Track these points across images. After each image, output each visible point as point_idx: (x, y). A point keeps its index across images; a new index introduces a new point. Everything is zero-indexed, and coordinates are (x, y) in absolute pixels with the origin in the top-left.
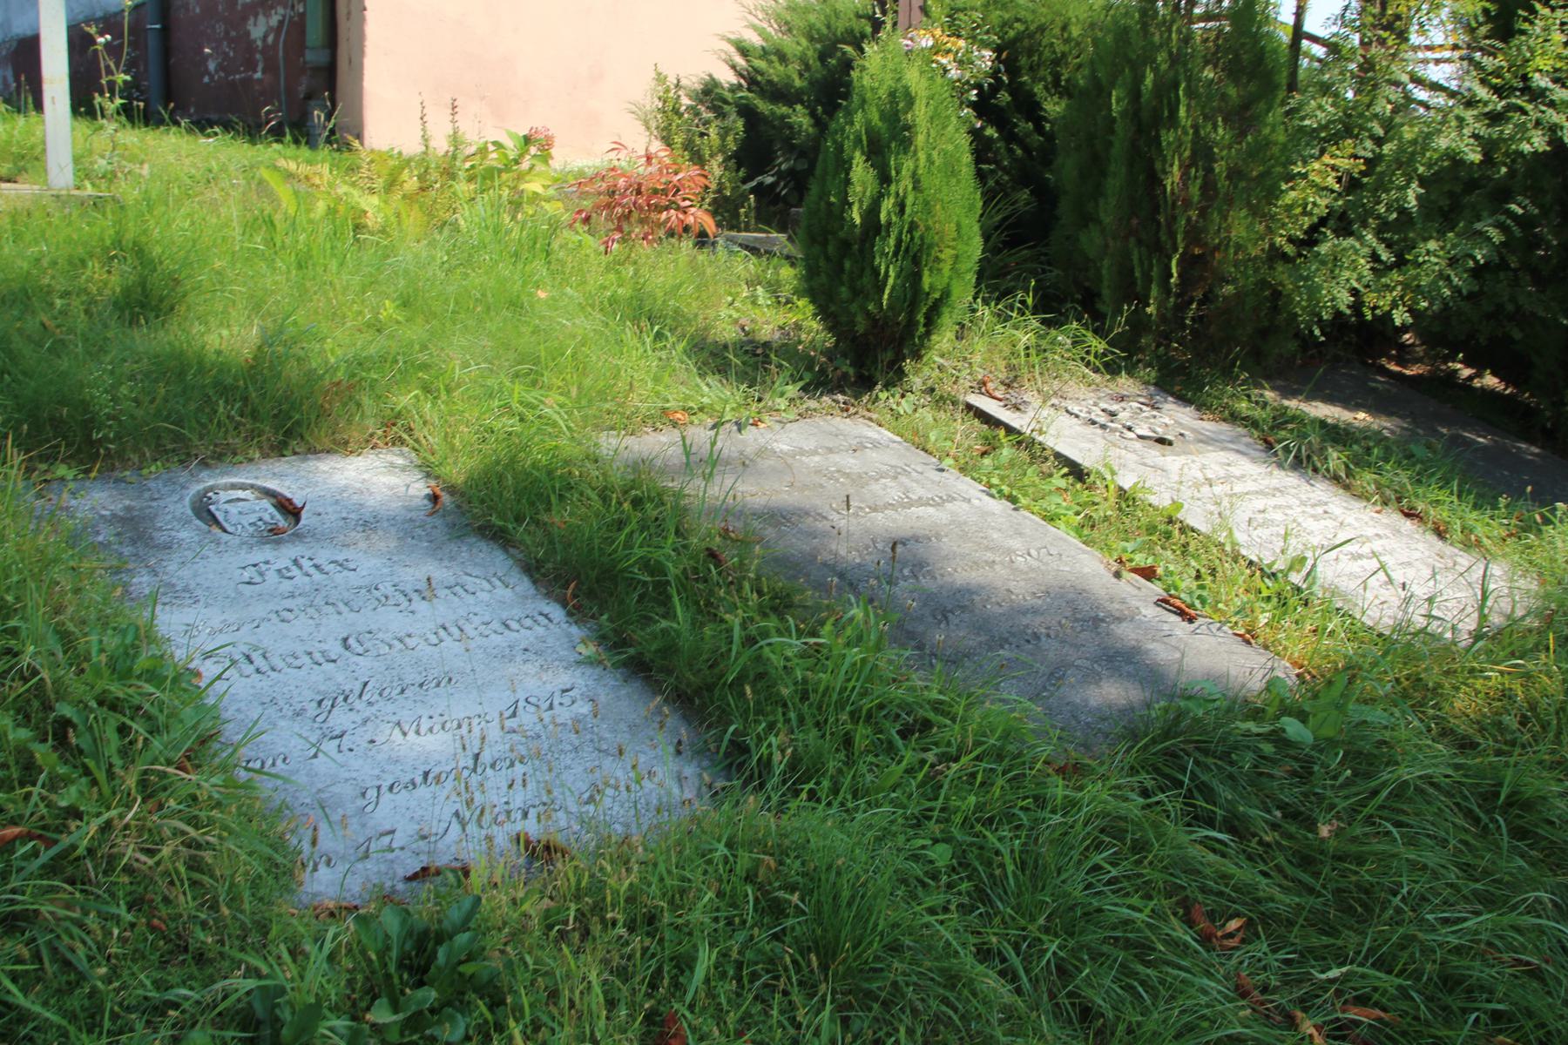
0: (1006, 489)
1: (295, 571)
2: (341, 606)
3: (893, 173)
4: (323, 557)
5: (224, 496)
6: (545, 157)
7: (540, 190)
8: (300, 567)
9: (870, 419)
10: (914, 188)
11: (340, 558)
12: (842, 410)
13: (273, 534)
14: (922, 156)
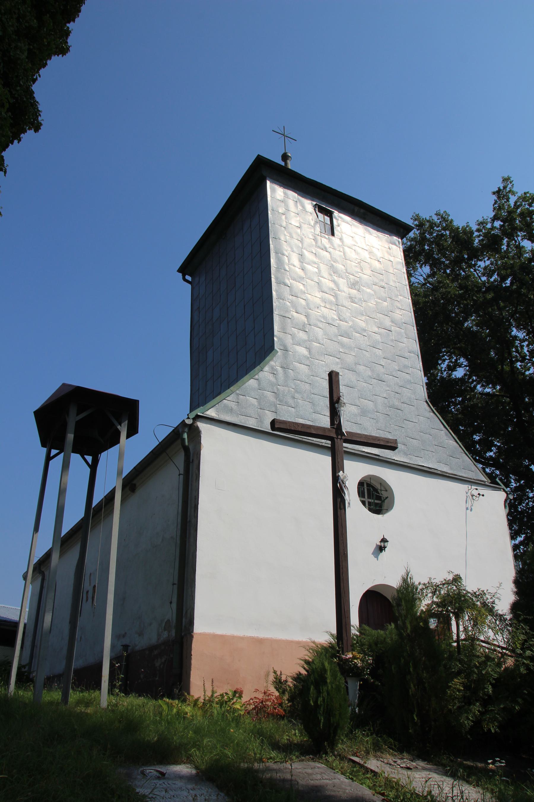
0: (351, 776)
1: (163, 784)
2: (173, 790)
3: (321, 691)
4: (170, 782)
5: (148, 771)
6: (240, 697)
7: (239, 707)
8: (165, 784)
9: (320, 762)
10: (328, 695)
11: (174, 783)
12: (312, 760)
13: (159, 778)
14: (330, 686)
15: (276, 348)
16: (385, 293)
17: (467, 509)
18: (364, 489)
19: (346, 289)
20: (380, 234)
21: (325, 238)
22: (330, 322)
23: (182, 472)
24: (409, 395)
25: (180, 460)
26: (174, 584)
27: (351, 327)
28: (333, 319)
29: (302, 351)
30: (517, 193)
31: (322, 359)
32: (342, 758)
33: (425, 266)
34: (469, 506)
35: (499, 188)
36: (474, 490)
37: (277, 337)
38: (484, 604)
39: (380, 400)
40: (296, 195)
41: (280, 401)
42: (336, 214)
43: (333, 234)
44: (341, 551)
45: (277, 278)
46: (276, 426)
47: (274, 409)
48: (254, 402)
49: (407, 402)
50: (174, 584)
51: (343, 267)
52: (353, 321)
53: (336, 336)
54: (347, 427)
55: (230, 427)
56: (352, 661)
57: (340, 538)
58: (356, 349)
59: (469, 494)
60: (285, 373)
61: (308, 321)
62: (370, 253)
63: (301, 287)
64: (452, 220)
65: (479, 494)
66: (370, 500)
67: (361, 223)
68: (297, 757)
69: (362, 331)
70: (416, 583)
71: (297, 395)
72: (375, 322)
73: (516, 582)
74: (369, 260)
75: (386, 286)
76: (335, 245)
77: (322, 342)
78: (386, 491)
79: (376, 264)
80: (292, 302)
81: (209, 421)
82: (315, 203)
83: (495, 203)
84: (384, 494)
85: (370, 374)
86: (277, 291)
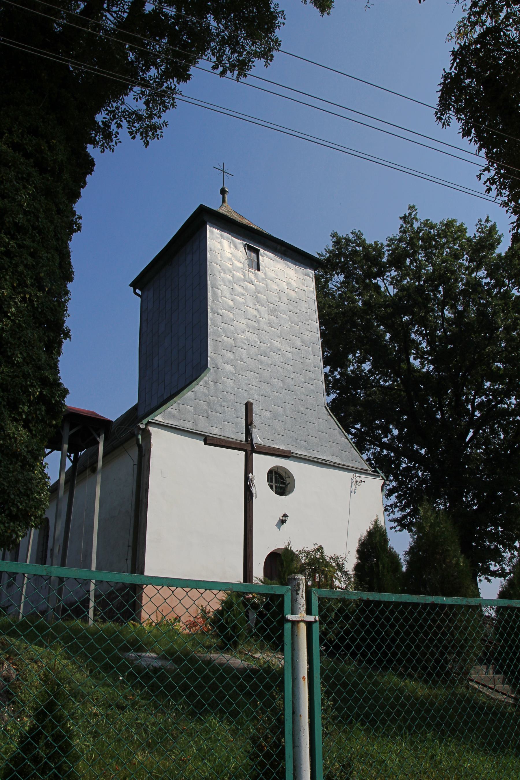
15: (209, 366)
16: (298, 318)
17: (351, 492)
18: (272, 476)
19: (266, 316)
20: (297, 268)
21: (252, 272)
22: (253, 344)
23: (136, 463)
24: (312, 402)
25: (134, 452)
26: (129, 546)
27: (268, 347)
28: (255, 342)
29: (229, 368)
30: (420, 219)
31: (244, 374)
32: (240, 652)
33: (341, 275)
34: (353, 490)
35: (405, 215)
36: (358, 477)
37: (210, 358)
38: (338, 565)
39: (288, 406)
40: (230, 236)
41: (211, 408)
42: (262, 251)
43: (258, 269)
44: (248, 528)
45: (212, 309)
46: (208, 442)
47: (206, 415)
48: (191, 409)
49: (310, 408)
50: (129, 546)
51: (265, 297)
52: (271, 343)
53: (257, 355)
54: (258, 439)
55: (173, 430)
56: (252, 600)
57: (248, 519)
58: (271, 366)
59: (354, 480)
60: (216, 386)
61: (235, 344)
62: (288, 284)
63: (231, 316)
64: (364, 239)
65: (361, 481)
66: (277, 485)
67: (282, 258)
68: (214, 651)
69: (277, 351)
70: (294, 551)
71: (224, 404)
72: (288, 343)
73: (358, 551)
74: (287, 291)
75: (299, 312)
76: (260, 279)
77: (245, 360)
78: (289, 478)
79: (292, 293)
80: (223, 328)
81: (157, 426)
82: (245, 243)
83: (401, 227)
84: (288, 480)
85: (282, 385)
86: (211, 320)
